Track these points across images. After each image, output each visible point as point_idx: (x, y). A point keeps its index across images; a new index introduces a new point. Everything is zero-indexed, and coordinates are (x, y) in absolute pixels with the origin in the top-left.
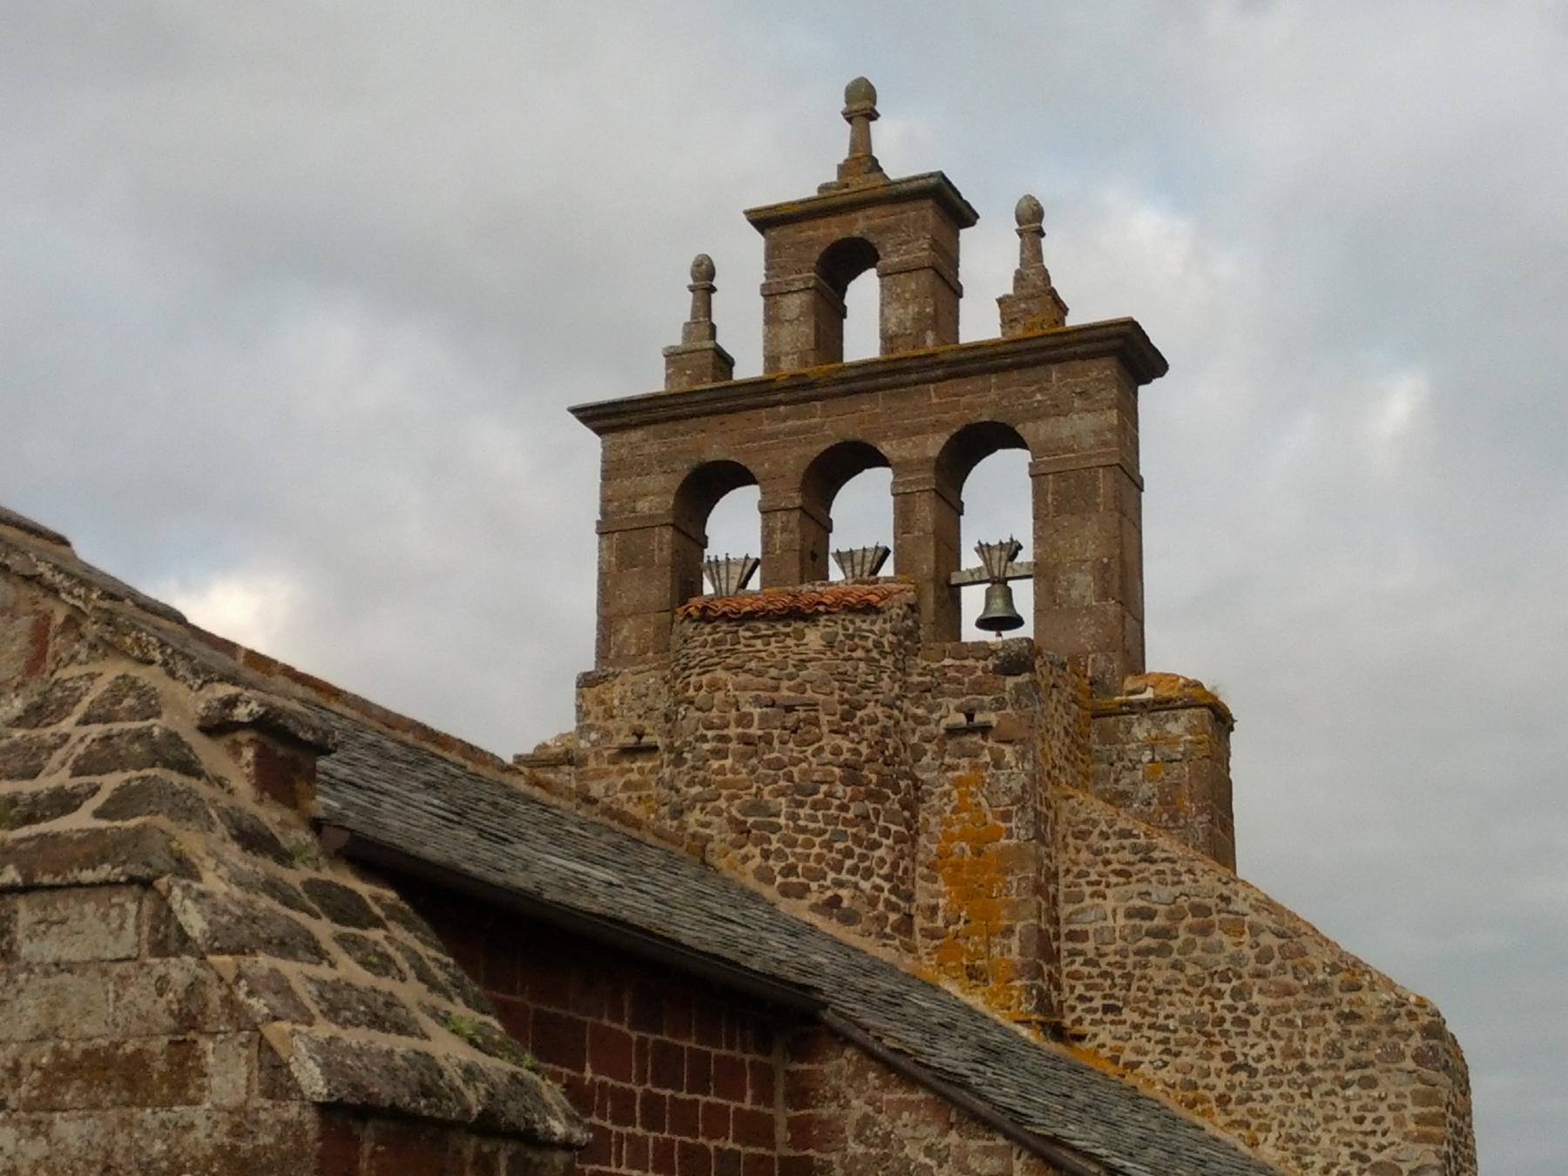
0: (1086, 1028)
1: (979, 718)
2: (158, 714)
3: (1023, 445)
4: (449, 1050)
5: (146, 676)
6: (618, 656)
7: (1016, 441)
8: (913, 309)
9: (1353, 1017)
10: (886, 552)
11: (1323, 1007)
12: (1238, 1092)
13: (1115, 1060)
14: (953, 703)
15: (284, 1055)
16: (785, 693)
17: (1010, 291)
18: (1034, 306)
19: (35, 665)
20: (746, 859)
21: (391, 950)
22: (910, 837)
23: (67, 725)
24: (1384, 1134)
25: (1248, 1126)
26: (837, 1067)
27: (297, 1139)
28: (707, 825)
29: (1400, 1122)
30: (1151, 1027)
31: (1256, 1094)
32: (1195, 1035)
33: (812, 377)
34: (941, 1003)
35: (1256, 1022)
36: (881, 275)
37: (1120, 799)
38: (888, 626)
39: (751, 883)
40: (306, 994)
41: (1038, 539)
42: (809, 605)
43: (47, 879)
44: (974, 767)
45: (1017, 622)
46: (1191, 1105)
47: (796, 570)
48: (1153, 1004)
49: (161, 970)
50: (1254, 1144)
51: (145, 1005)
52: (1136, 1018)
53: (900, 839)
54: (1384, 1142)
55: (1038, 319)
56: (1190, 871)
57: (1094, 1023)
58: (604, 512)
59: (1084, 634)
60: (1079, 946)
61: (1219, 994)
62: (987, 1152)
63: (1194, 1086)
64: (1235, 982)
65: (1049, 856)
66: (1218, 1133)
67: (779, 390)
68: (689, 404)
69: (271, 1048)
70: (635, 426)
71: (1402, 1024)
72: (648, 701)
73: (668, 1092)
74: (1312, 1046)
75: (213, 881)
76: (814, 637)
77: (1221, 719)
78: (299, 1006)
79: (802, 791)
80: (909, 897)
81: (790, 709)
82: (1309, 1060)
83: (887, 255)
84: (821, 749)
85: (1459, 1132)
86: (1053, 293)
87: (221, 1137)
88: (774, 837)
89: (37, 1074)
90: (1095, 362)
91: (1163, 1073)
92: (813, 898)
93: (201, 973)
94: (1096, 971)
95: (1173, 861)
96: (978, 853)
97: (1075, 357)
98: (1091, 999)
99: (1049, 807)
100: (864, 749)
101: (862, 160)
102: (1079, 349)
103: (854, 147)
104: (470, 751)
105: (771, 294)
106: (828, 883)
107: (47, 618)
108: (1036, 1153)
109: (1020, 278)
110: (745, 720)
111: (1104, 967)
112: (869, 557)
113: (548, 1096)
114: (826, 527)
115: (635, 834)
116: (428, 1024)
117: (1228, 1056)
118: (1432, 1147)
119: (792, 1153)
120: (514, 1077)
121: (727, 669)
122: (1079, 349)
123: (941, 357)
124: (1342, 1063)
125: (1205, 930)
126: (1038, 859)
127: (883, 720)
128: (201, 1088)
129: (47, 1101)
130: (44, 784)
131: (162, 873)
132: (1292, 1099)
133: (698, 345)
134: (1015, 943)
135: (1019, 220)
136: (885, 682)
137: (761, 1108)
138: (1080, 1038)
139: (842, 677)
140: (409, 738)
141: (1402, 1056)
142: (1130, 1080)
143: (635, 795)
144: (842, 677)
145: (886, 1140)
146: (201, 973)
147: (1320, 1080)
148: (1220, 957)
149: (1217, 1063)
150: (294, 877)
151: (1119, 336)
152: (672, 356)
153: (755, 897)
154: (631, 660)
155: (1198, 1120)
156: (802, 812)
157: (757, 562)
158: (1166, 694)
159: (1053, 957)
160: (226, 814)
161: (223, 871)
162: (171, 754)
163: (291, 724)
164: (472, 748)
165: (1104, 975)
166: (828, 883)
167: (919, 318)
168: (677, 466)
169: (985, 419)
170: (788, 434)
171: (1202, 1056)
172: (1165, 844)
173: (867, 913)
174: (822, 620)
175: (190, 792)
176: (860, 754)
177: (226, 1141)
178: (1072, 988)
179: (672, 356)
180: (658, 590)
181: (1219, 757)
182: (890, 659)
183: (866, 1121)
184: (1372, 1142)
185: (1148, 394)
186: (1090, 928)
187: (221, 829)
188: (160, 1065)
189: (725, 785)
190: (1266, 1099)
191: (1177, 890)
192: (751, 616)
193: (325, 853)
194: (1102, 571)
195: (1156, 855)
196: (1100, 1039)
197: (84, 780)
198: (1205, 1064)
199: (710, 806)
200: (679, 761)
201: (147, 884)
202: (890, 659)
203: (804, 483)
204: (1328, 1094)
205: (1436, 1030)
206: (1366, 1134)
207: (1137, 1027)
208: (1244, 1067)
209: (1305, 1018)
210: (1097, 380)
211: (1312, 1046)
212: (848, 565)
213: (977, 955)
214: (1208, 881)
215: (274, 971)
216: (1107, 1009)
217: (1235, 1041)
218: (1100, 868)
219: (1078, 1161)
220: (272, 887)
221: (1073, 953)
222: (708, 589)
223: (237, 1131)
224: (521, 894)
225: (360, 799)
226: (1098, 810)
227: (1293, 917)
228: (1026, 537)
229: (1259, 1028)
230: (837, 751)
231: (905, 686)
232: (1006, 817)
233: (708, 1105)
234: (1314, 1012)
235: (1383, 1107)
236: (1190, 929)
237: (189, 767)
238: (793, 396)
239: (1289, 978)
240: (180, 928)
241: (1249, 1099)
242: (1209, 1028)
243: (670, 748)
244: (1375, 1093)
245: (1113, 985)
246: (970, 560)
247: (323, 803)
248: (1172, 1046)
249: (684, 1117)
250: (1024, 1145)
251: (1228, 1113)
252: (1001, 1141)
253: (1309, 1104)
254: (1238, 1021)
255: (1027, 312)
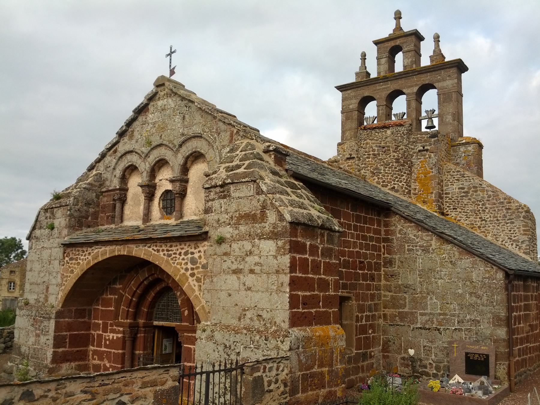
0: (449, 213)
1: (426, 148)
2: (255, 149)
3: (436, 88)
4: (314, 213)
5: (252, 142)
6: (346, 139)
7: (434, 88)
8: (410, 60)
9: (509, 209)
10: (405, 113)
11: (502, 207)
12: (483, 225)
13: (455, 219)
14: (420, 145)
15: (283, 213)
16: (383, 144)
17: (432, 54)
18: (438, 57)
19: (231, 141)
20: (374, 179)
21: (302, 194)
22: (410, 174)
23: (238, 152)
24: (516, 234)
25: (485, 232)
26: (394, 219)
27: (285, 229)
28: (365, 173)
29: (519, 231)
30: (463, 212)
31: (487, 226)
32: (473, 214)
33: (388, 76)
34: (417, 208)
35: (487, 211)
36: (403, 53)
37: (457, 164)
38: (405, 129)
39: (375, 184)
40: (286, 202)
41: (439, 109)
42: (388, 125)
43: (236, 181)
44: (425, 158)
45: (434, 127)
46: (472, 228)
47: (385, 118)
48: (464, 207)
49: (258, 198)
50: (486, 236)
51: (255, 204)
52: (460, 210)
53: (408, 174)
54: (516, 235)
55: (439, 60)
56: (473, 179)
57: (451, 212)
58: (342, 109)
59: (450, 129)
60: (448, 196)
61: (479, 205)
62: (427, 235)
63: (473, 224)
64: (483, 202)
65: (441, 177)
66: (478, 234)
67: (381, 79)
68: (360, 84)
69: (280, 212)
70: (349, 90)
71: (520, 210)
72: (352, 148)
73: (359, 224)
74: (500, 215)
75: (267, 181)
76: (389, 132)
77: (480, 146)
78: (285, 204)
79: (386, 165)
80: (410, 187)
81: (384, 148)
82: (499, 218)
83: (404, 48)
84: (391, 156)
85: (533, 233)
86: (442, 54)
87: (271, 229)
88: (380, 175)
89: (236, 218)
90: (452, 69)
91: (466, 222)
92: (389, 187)
93: (266, 198)
94: (451, 201)
95: (469, 177)
96: (425, 177)
97: (447, 68)
98: (450, 207)
99: (441, 166)
100: (400, 155)
101: (398, 28)
102: (448, 66)
103: (396, 25)
104: (315, 159)
105: (378, 59)
106: (392, 184)
107: (233, 132)
108: (438, 236)
109: (434, 51)
110: (374, 150)
111: (453, 200)
112: (401, 115)
113: (334, 222)
114: (391, 109)
115: (350, 175)
116: (310, 208)
117: (480, 218)
118: (527, 236)
119: (385, 237)
120: (327, 218)
121: (370, 140)
122: (448, 66)
123: (417, 70)
124: (506, 219)
125: (476, 191)
126: (439, 177)
127: (404, 149)
128: (267, 220)
129: (238, 224)
130: (234, 164)
131: (258, 179)
132: (495, 226)
133: (362, 71)
134: (433, 195)
135: (434, 38)
136: (405, 141)
137: (378, 228)
138: (448, 215)
139: (395, 140)
140: (303, 156)
141: (520, 217)
142: (459, 223)
143: (350, 168)
144: (395, 140)
145: (405, 234)
146: (266, 198)
147: (502, 223)
148: (479, 197)
149: (478, 219)
150: (283, 180)
151: (457, 63)
152: (357, 74)
153: (376, 187)
154: (349, 140)
155: (474, 231)
156: (386, 169)
157: (376, 117)
158: (468, 141)
159: (442, 198)
160: (269, 168)
161: (269, 179)
162: (258, 157)
163: (281, 150)
164: (316, 158)
165: (453, 202)
166: (392, 184)
167: (412, 61)
168: (358, 98)
169: (427, 83)
170: (383, 89)
171: (475, 218)
172: (467, 173)
173: (401, 190)
174: (391, 128)
175: (262, 164)
176: (399, 156)
177: (272, 230)
178: (446, 204)
179: (357, 74)
180: (354, 124)
181: (480, 154)
182: (406, 136)
183: (401, 230)
184: (513, 235)
185: (464, 75)
186: (450, 192)
187: (268, 171)
188: (259, 216)
189: (369, 164)
190: (489, 227)
191: (470, 183)
192: (375, 128)
193: (288, 176)
194: (453, 115)
195: (465, 176)
196: (452, 215)
197: (242, 162)
198: (475, 220)
199: (366, 169)
200: (359, 160)
201: (255, 181)
202: (406, 136)
203: (386, 99)
204: (503, 225)
205: (528, 211)
206: (511, 234)
207: (460, 212)
208: (484, 220)
209: (498, 210)
210: (453, 73)
211: (500, 215)
212: (396, 117)
213: (425, 198)
214: (477, 181)
215: (280, 197)
216: (454, 209)
217: (482, 215)
218: (453, 179)
219: (447, 237)
220: (278, 182)
221: (446, 197)
222: (365, 124)
223: (274, 228)
224: (327, 184)
225: (294, 167)
226: (452, 167)
227: (496, 188)
228: (436, 109)
229: (488, 212)
230: (394, 156)
231: (409, 142)
232: (432, 169)
233: (367, 227)
234: (500, 208)
235: (516, 228)
236: (473, 191)
237: (262, 159)
238: (383, 81)
239: (495, 201)
240: (261, 189)
241: (485, 227)
242: (476, 212)
243: (357, 157)
244: (514, 225)
245: (455, 204)
246: (424, 114)
247: (287, 167)
248: (468, 216)
249: (362, 229)
250: (435, 234)
251: (480, 230)
252: (430, 233)
253: (499, 227)
254: (483, 211)
255: (436, 59)
